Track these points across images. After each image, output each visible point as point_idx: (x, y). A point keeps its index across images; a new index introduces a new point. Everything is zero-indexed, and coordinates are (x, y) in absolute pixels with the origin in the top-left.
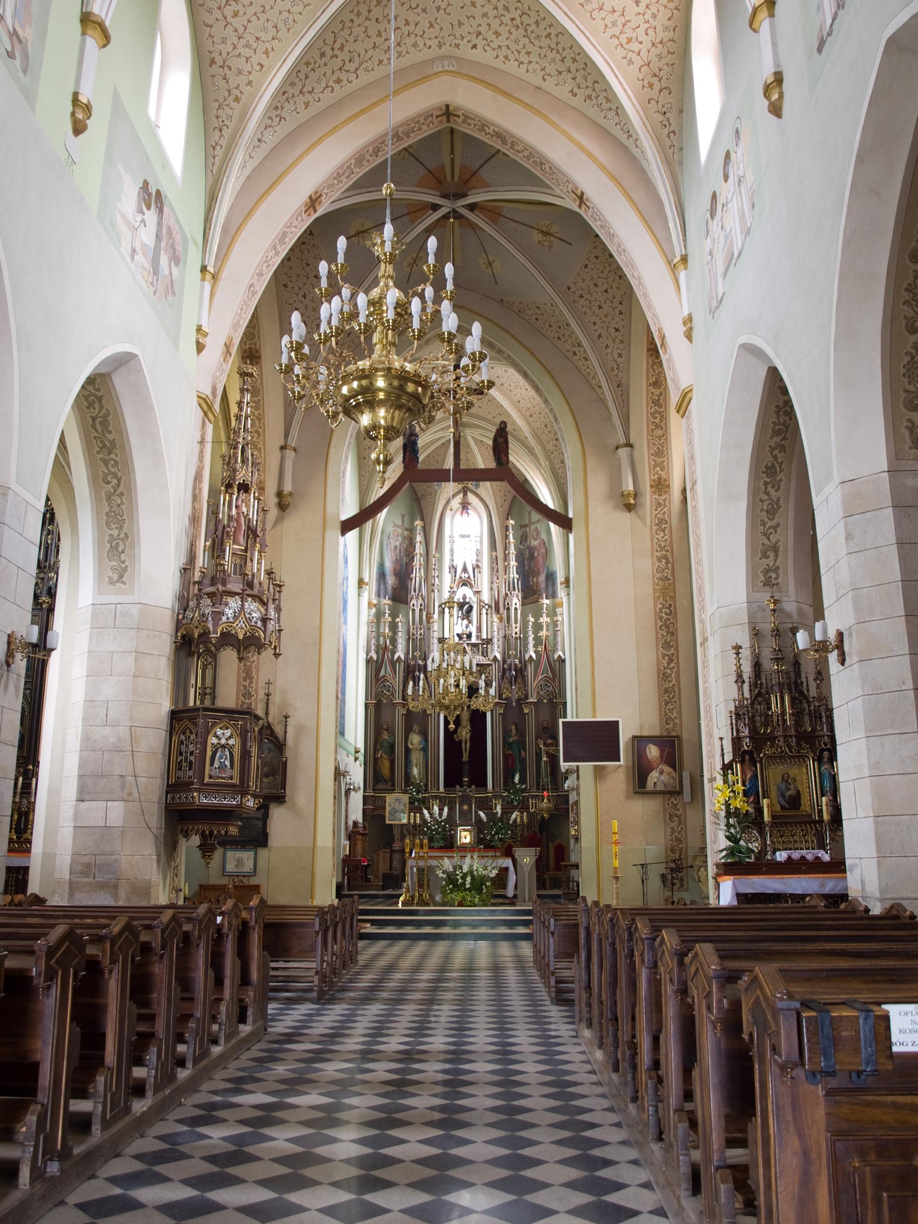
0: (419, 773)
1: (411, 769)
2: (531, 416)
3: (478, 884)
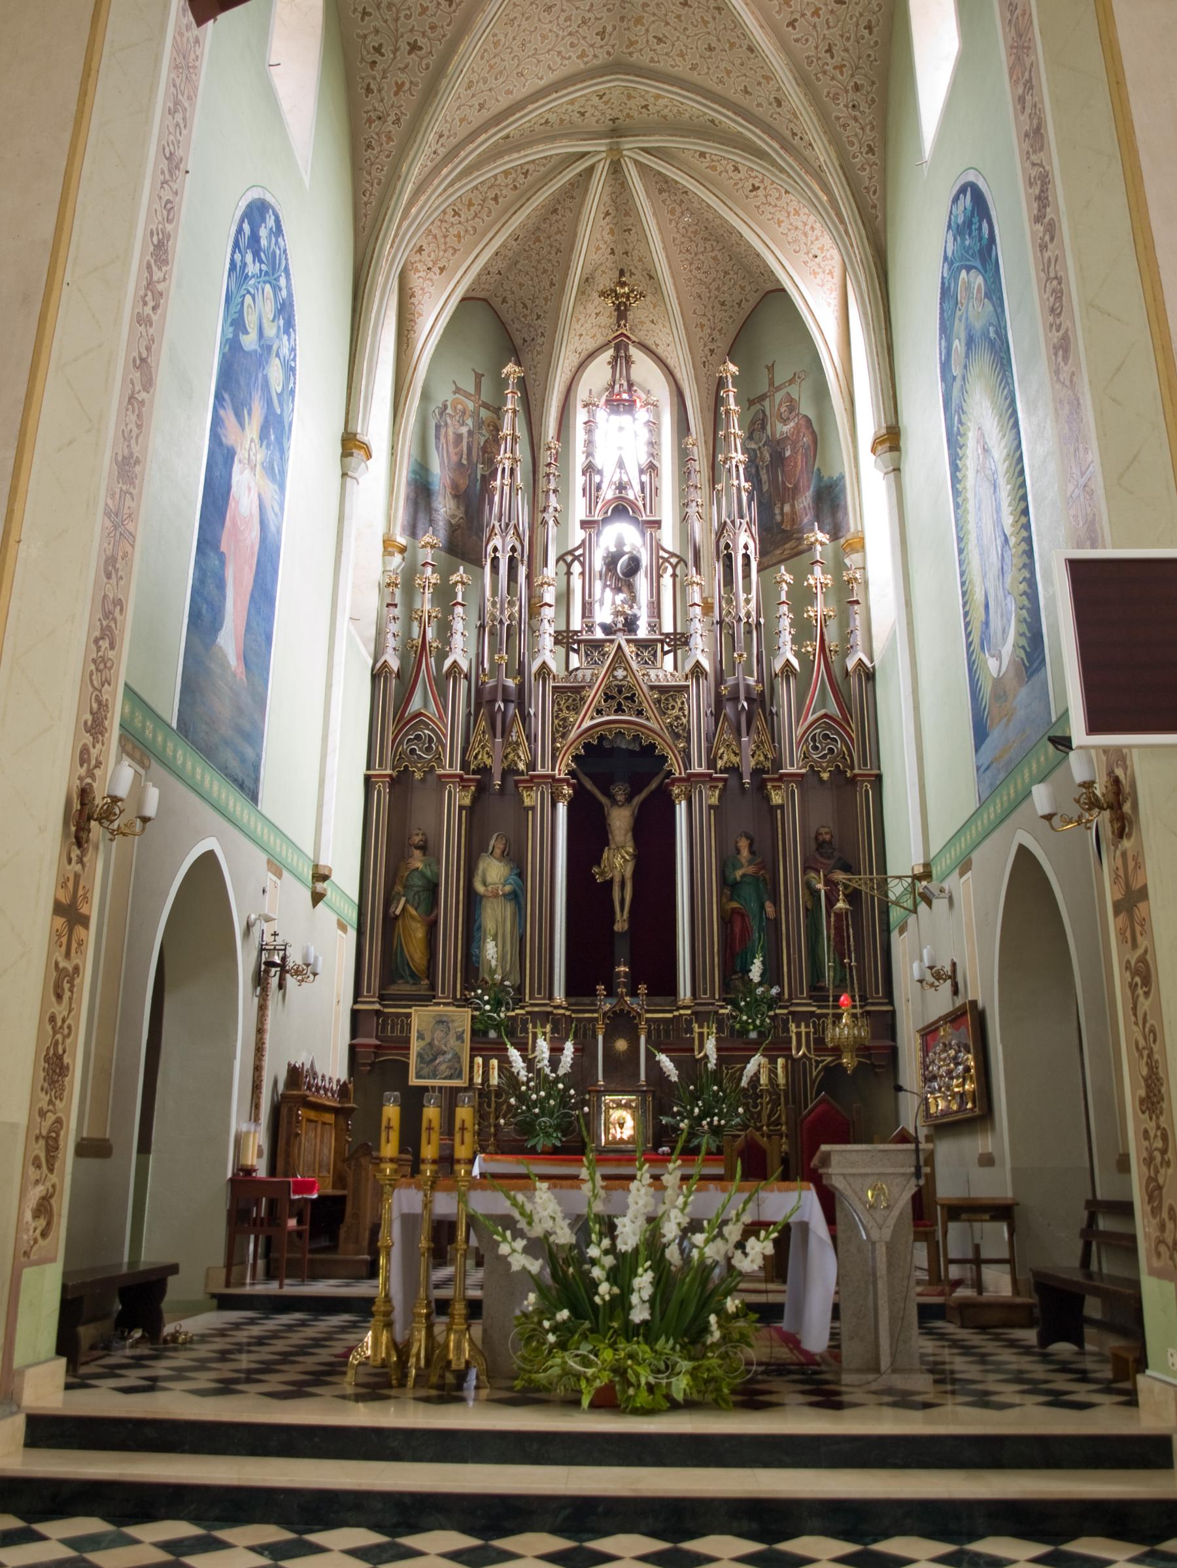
0: (502, 958)
1: (481, 948)
2: (792, 24)
3: (687, 1302)
